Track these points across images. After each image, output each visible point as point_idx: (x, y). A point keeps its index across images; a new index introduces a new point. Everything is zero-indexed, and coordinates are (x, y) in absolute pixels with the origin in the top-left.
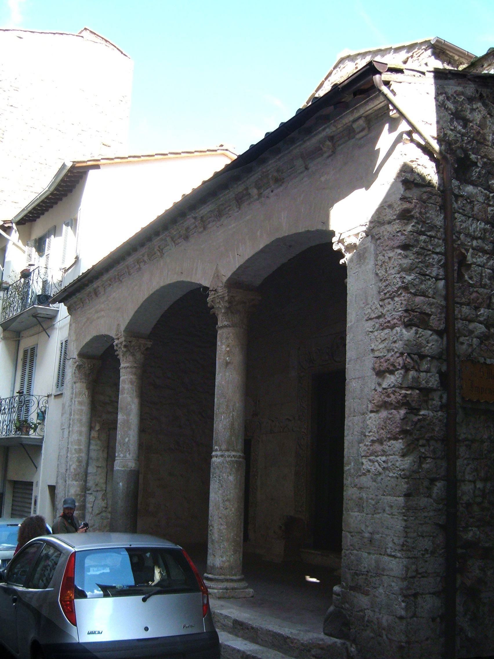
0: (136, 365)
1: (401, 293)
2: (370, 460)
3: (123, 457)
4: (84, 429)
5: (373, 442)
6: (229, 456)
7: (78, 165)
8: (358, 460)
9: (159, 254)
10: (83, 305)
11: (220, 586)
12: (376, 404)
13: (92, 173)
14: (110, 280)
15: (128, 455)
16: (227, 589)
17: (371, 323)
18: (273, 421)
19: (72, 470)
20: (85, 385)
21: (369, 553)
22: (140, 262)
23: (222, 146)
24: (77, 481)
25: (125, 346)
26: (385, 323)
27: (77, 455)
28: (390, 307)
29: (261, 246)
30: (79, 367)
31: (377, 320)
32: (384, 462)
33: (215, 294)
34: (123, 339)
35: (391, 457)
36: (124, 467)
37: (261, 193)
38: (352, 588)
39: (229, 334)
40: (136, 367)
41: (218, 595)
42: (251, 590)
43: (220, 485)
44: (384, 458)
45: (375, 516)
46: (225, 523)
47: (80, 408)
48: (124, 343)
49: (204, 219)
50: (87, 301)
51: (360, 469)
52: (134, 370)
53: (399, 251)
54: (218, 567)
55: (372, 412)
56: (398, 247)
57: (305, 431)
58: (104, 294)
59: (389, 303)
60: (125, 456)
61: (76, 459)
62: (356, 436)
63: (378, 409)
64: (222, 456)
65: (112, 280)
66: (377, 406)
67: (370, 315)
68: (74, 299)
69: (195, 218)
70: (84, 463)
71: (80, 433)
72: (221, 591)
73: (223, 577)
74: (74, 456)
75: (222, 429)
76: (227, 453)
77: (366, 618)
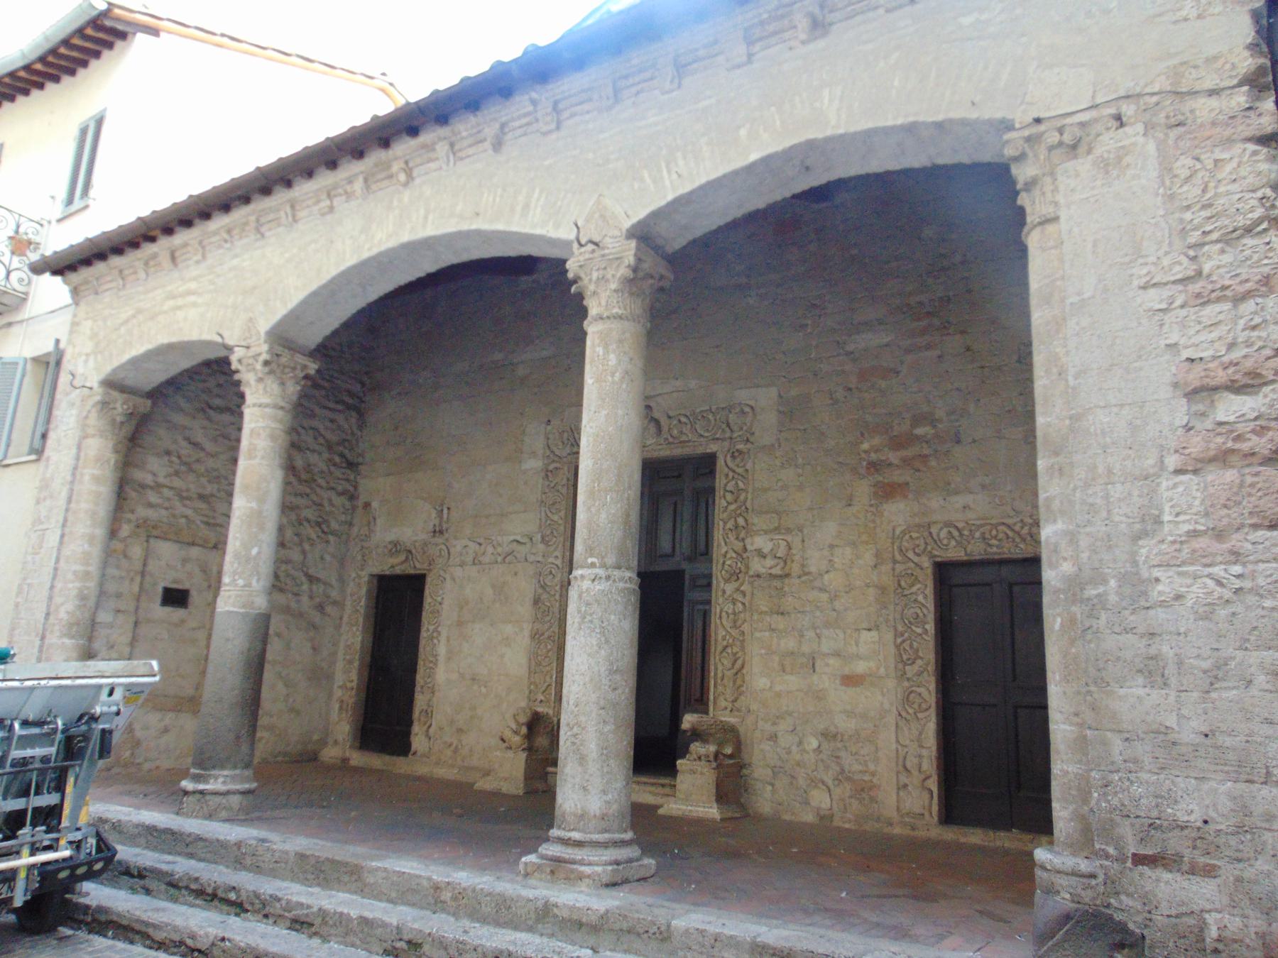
0: (283, 404)
1: (1265, 230)
2: (1179, 574)
3: (245, 586)
4: (100, 532)
5: (1194, 534)
6: (622, 579)
7: (117, 11)
8: (1138, 573)
9: (402, 177)
10: (124, 285)
11: (604, 858)
12: (1193, 456)
13: (141, 38)
14: (229, 231)
15: (254, 582)
16: (617, 863)
17: (1166, 292)
18: (480, 544)
19: (63, 615)
20: (110, 445)
21: (1200, 779)
22: (335, 196)
23: (384, 74)
24: (72, 637)
25: (266, 363)
26: (1213, 291)
27: (78, 584)
28: (1227, 258)
29: (754, 157)
30: (105, 405)
31: (1180, 287)
32: (1238, 576)
33: (593, 251)
34: (265, 347)
35: (1262, 566)
36: (244, 607)
37: (753, 55)
38: (1139, 860)
39: (624, 333)
40: (282, 408)
41: (604, 881)
42: (652, 861)
43: (603, 639)
44: (1237, 569)
45: (1214, 695)
46: (612, 720)
47: (94, 488)
48: (265, 356)
49: (561, 106)
50: (142, 275)
51: (1144, 594)
52: (280, 413)
53: (1251, 147)
54: (595, 816)
55: (1178, 472)
56: (1249, 140)
57: (559, 562)
58: (198, 262)
59: (1223, 251)
60: (248, 585)
61: (75, 592)
62: (1123, 526)
63: (1199, 466)
64: (608, 578)
65: (235, 232)
66: (1201, 461)
67: (1152, 278)
68: (85, 273)
69: (534, 103)
70: (91, 603)
71: (91, 539)
72: (610, 868)
73: (607, 836)
74: (70, 586)
75: (606, 522)
76: (617, 573)
77: (1213, 932)
